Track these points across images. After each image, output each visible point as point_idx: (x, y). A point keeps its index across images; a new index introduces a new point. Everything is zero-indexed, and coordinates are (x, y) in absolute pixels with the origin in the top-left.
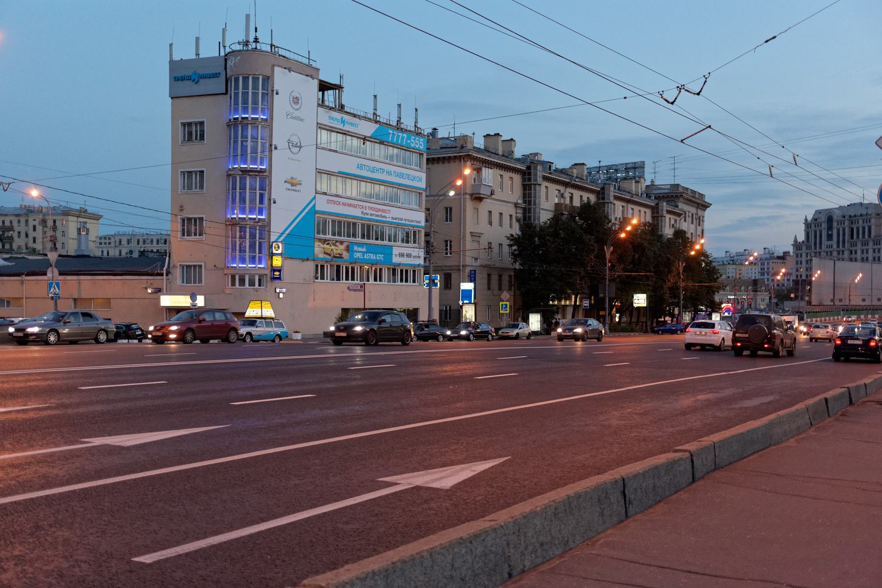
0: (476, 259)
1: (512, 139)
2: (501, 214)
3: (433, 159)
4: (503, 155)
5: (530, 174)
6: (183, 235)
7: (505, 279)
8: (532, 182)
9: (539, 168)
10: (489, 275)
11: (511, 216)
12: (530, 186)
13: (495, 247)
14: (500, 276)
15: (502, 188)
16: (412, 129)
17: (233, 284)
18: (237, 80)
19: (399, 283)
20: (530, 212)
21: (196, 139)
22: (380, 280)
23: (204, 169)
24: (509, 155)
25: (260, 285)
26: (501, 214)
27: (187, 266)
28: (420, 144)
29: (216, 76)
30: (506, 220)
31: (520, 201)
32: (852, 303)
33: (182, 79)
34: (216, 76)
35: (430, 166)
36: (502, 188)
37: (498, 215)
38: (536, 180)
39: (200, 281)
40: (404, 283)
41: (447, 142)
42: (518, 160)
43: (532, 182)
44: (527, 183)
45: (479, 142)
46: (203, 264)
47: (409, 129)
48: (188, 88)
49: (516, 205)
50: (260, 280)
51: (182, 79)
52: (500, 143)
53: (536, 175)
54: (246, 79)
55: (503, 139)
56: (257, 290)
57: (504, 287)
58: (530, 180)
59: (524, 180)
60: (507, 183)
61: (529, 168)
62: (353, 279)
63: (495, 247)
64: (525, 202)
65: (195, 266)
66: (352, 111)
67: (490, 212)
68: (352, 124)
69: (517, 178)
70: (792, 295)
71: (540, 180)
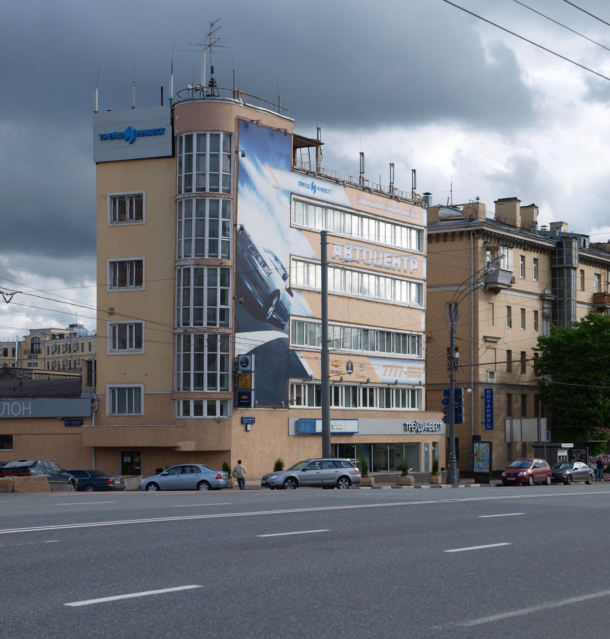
0: (492, 374)
1: (533, 205)
2: (523, 310)
3: (438, 235)
4: (522, 228)
5: (561, 253)
6: (114, 347)
7: (531, 400)
8: (565, 264)
9: (575, 244)
10: (509, 396)
11: (536, 312)
12: (561, 269)
13: (516, 356)
14: (524, 397)
15: (523, 274)
16: (409, 197)
17: (187, 412)
18: (189, 138)
19: (362, 408)
20: (561, 306)
21: (131, 217)
22: (371, 405)
23: (143, 258)
24: (529, 226)
25: (221, 414)
26: (523, 310)
27: (119, 389)
28: (421, 217)
29: (159, 132)
30: (530, 317)
31: (548, 292)
32: (527, 410)
33: (113, 137)
34: (159, 132)
35: (434, 244)
36: (523, 274)
37: (533, 314)
38: (571, 262)
39: (138, 410)
40: (368, 408)
41: (453, 213)
42: (543, 233)
43: (565, 264)
44: (558, 266)
45: (490, 212)
46: (142, 386)
47: (404, 197)
48: (120, 150)
49: (542, 298)
50: (222, 407)
51: (113, 137)
52: (518, 210)
53: (570, 255)
54: (201, 137)
55: (522, 204)
56: (218, 421)
57: (528, 412)
58: (561, 261)
59: (552, 262)
60: (530, 265)
61: (559, 245)
62: (371, 405)
63: (516, 356)
64: (554, 292)
65: (130, 389)
66: (333, 176)
67: (509, 308)
68: (323, 190)
69: (543, 260)
70: (241, 299)
71: (575, 261)
